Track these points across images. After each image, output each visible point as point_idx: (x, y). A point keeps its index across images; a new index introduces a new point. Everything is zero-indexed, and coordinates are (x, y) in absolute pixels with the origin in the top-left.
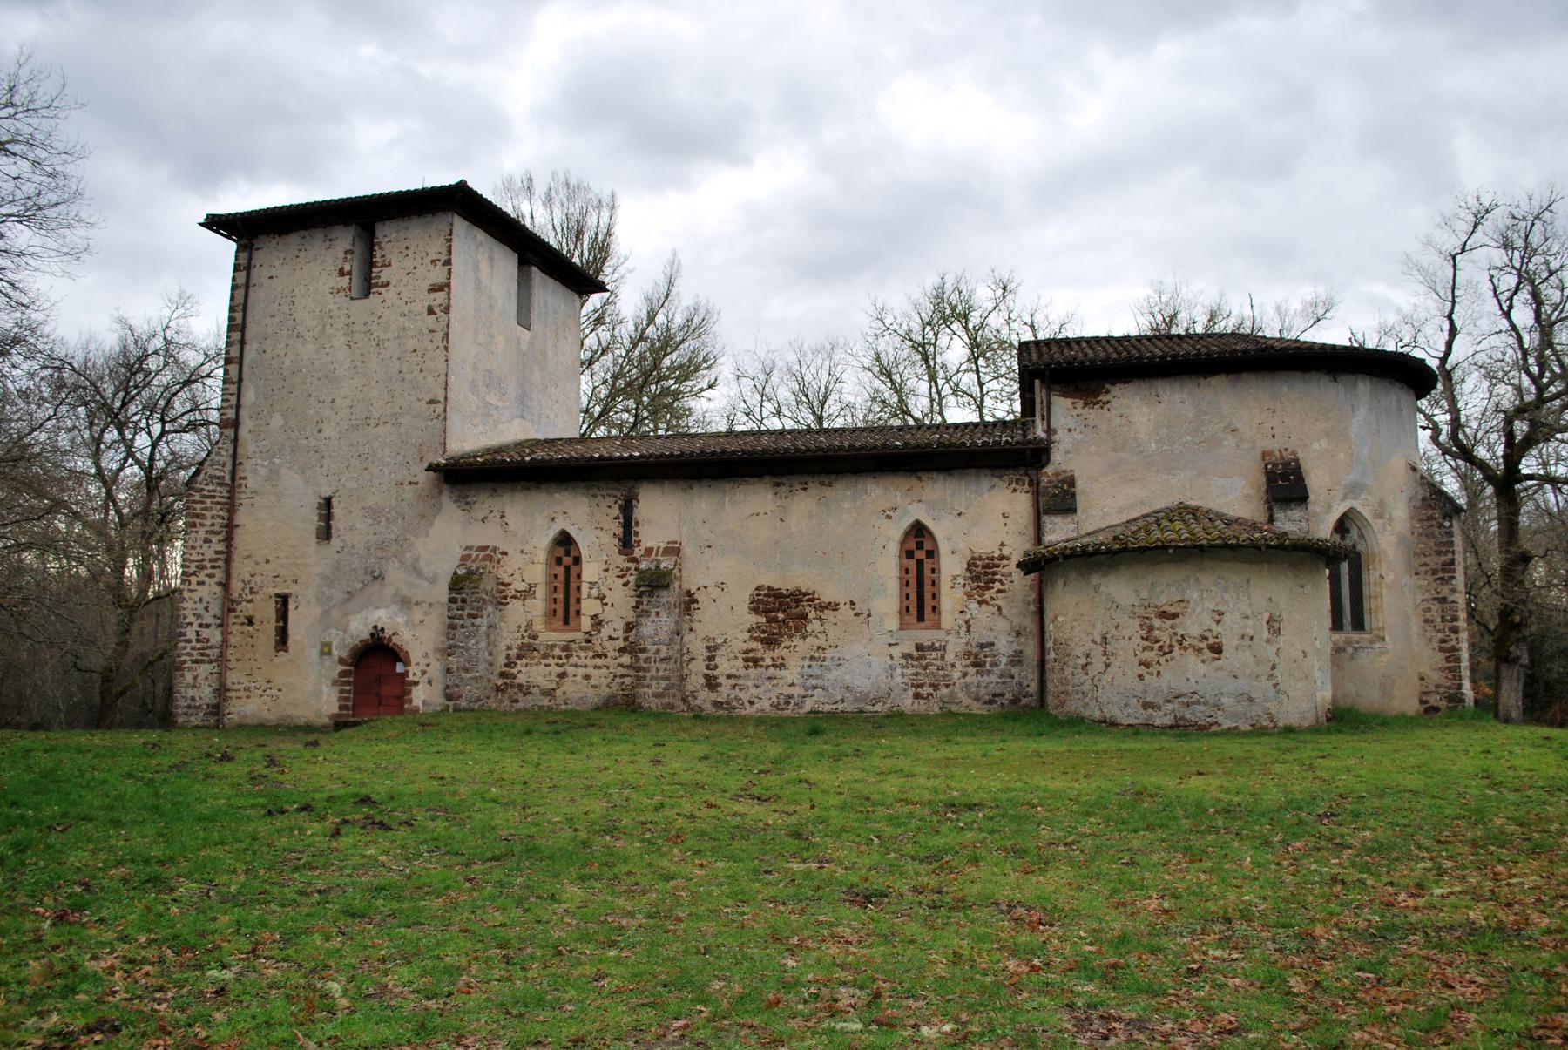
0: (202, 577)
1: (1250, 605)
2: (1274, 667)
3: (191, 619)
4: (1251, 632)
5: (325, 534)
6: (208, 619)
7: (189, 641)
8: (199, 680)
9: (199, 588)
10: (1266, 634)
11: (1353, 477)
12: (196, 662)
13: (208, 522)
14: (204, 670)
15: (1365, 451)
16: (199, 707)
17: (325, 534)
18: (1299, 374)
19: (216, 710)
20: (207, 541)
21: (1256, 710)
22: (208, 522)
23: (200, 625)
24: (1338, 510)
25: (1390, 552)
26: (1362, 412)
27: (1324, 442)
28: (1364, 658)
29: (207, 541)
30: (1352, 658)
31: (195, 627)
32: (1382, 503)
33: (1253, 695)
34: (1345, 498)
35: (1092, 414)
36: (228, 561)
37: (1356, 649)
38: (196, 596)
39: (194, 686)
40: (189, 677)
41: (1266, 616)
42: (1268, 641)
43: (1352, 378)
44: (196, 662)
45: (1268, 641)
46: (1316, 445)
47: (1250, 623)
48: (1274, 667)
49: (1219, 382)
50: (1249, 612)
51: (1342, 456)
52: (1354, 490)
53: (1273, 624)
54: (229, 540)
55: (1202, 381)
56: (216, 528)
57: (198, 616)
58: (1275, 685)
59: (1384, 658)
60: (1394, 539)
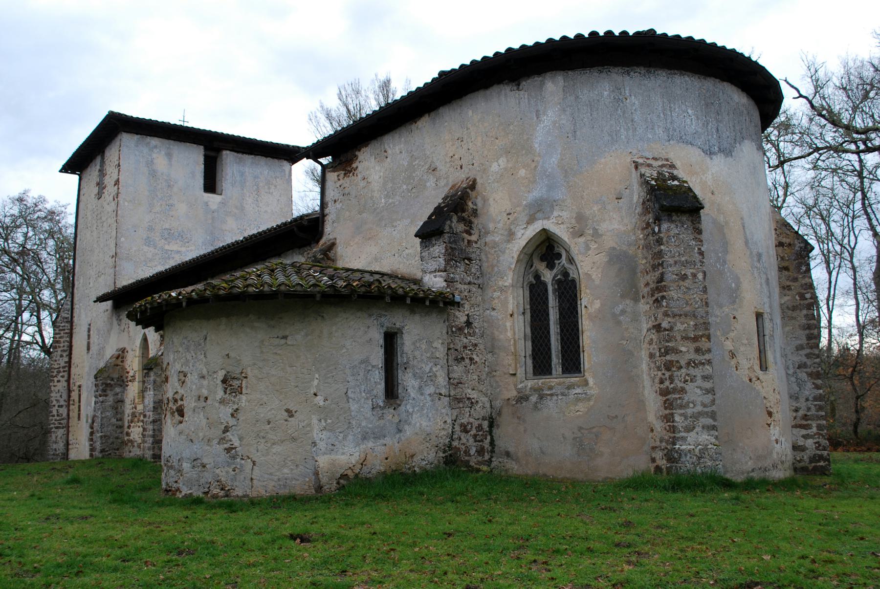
0: (59, 378)
1: (206, 364)
2: (226, 430)
3: (55, 403)
4: (205, 392)
5: (88, 349)
6: (62, 403)
7: (53, 416)
8: (58, 439)
9: (58, 384)
10: (220, 394)
11: (536, 193)
12: (57, 428)
13: (62, 345)
14: (61, 432)
15: (554, 160)
16: (58, 455)
17: (88, 349)
18: (481, 93)
19: (65, 456)
20: (62, 356)
21: (208, 477)
22: (62, 345)
23: (59, 406)
24: (525, 235)
25: (596, 276)
26: (550, 116)
27: (502, 161)
28: (551, 406)
29: (62, 356)
30: (536, 407)
31: (56, 407)
32: (580, 218)
33: (205, 461)
34: (531, 220)
35: (346, 182)
36: (70, 367)
37: (541, 397)
38: (56, 389)
39: (56, 443)
40: (54, 436)
41: (221, 375)
42: (222, 402)
43: (537, 79)
44: (57, 428)
45: (222, 402)
46: (495, 167)
47: (205, 382)
48: (226, 430)
49: (424, 123)
50: (205, 372)
51: (522, 172)
52: (538, 209)
53: (231, 384)
54: (70, 355)
55: (414, 126)
56: (65, 348)
57: (57, 401)
58: (228, 450)
59: (582, 407)
60: (603, 258)
